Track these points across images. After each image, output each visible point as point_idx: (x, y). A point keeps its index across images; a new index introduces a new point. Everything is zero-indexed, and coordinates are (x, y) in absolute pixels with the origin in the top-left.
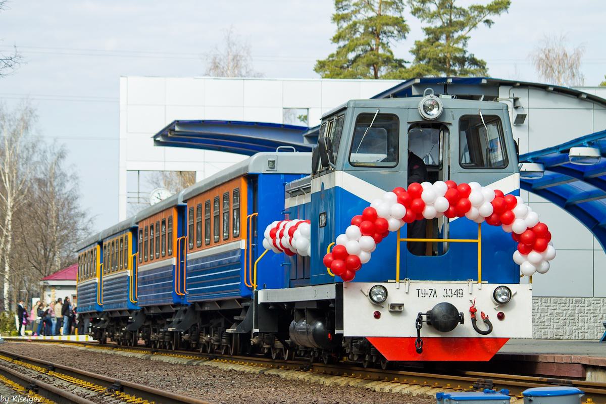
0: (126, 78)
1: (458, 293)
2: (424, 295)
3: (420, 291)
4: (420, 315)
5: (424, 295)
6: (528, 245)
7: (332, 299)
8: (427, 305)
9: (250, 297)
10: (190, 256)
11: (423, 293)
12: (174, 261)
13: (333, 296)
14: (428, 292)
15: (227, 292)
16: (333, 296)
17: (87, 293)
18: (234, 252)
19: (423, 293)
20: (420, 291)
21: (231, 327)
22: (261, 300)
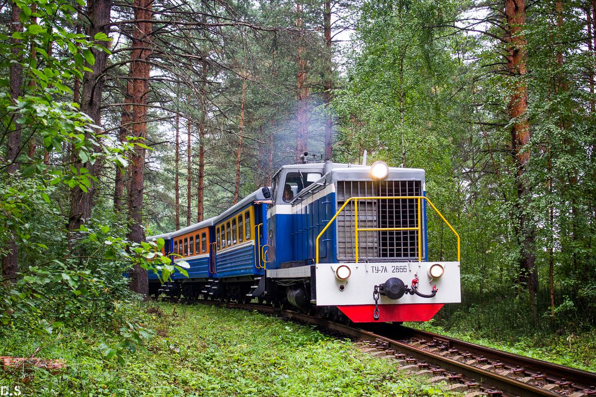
0: (308, 175)
1: (403, 270)
2: (377, 271)
3: (374, 268)
4: (376, 287)
5: (377, 271)
6: (256, 287)
7: (308, 277)
8: (382, 278)
9: (260, 272)
10: (218, 253)
11: (377, 269)
12: (208, 255)
13: (309, 275)
14: (380, 268)
15: (245, 269)
16: (309, 275)
17: (225, 261)
18: (250, 246)
19: (377, 269)
20: (374, 268)
21: (250, 292)
22: (268, 276)
